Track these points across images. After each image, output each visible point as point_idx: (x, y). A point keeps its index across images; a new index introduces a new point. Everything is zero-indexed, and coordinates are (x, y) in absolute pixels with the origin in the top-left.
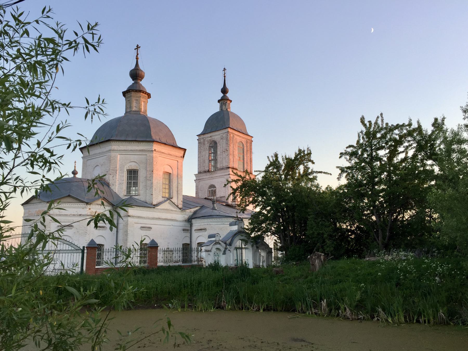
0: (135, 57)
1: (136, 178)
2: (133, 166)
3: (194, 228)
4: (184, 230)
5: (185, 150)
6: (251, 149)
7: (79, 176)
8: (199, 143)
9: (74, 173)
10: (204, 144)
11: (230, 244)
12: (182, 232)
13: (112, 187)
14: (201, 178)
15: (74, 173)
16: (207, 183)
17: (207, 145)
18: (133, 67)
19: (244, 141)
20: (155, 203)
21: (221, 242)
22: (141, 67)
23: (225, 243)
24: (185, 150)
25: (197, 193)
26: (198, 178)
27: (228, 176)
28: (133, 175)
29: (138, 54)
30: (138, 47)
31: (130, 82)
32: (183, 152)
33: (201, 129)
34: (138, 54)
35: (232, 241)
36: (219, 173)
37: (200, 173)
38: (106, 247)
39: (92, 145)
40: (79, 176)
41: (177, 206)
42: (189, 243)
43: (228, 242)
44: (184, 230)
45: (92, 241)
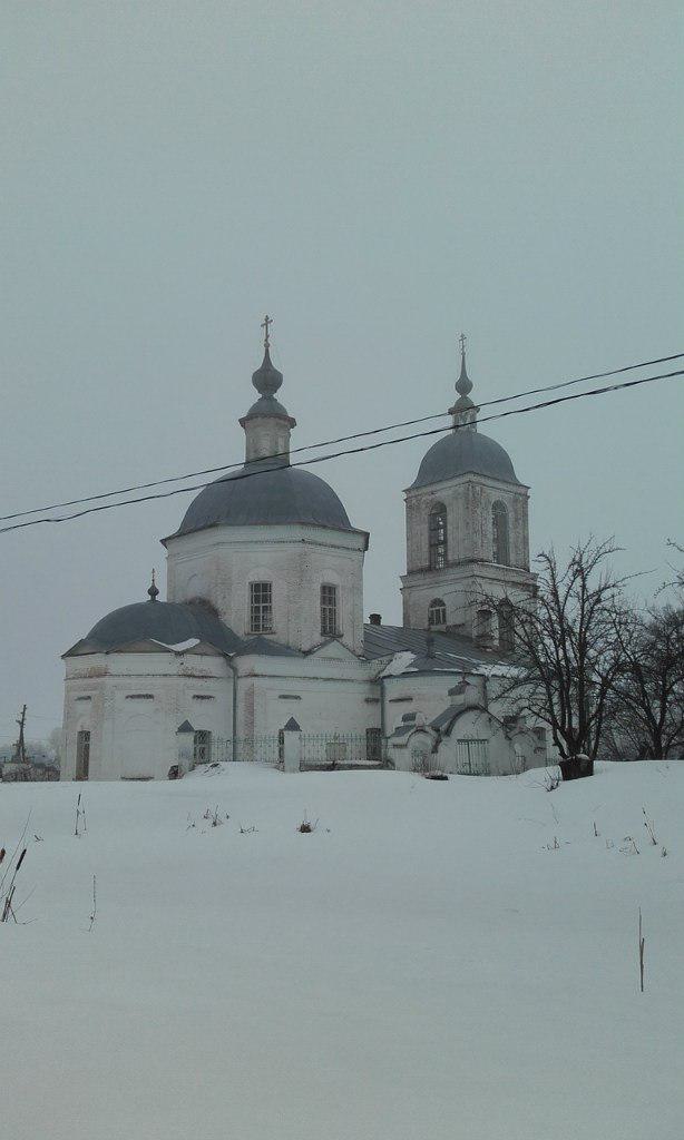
0: (263, 342)
1: (267, 599)
2: (260, 575)
3: (389, 697)
4: (367, 700)
5: (367, 535)
6: (525, 515)
7: (162, 598)
8: (410, 508)
9: (153, 592)
10: (419, 508)
11: (448, 732)
12: (366, 705)
13: (223, 619)
14: (413, 583)
15: (153, 592)
16: (426, 595)
17: (425, 514)
18: (259, 366)
19: (506, 498)
20: (306, 647)
21: (427, 729)
22: (276, 364)
23: (437, 730)
24: (367, 535)
25: (406, 617)
26: (408, 584)
27: (471, 580)
28: (261, 592)
29: (268, 336)
30: (267, 321)
31: (255, 396)
32: (361, 540)
33: (410, 476)
34: (268, 336)
35: (452, 724)
36: (454, 573)
37: (410, 572)
38: (215, 735)
39: (181, 534)
40: (162, 598)
41: (353, 652)
42: (380, 727)
43: (443, 728)
44: (367, 700)
45: (251, 584)
